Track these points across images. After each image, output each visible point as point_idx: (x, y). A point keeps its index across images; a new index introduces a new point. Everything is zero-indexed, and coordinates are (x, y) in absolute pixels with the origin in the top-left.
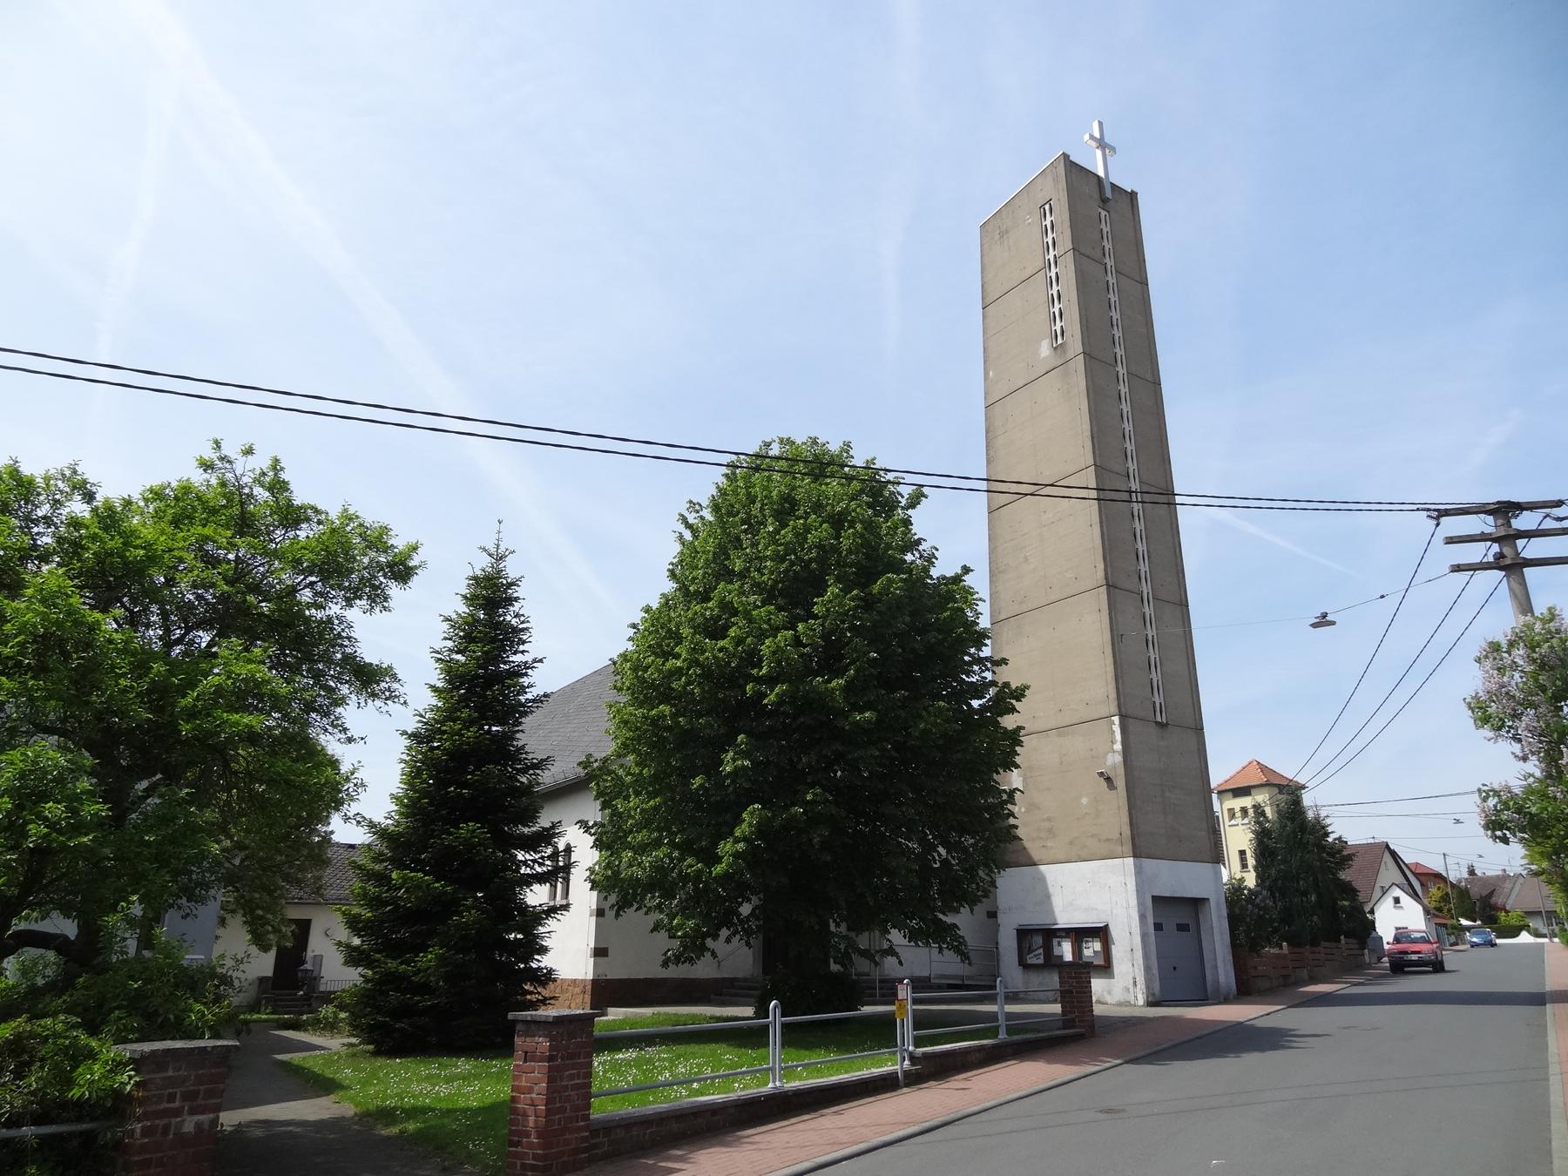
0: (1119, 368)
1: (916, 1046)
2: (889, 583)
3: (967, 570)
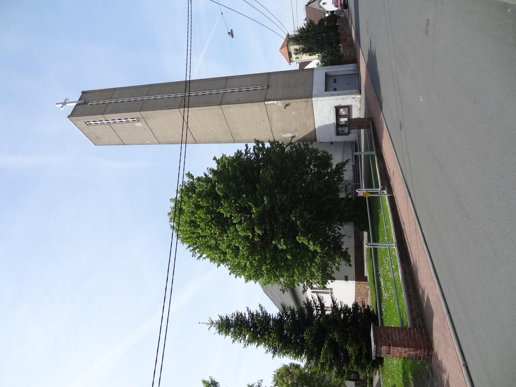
0: (145, 99)
1: (378, 187)
2: (219, 189)
3: (215, 159)
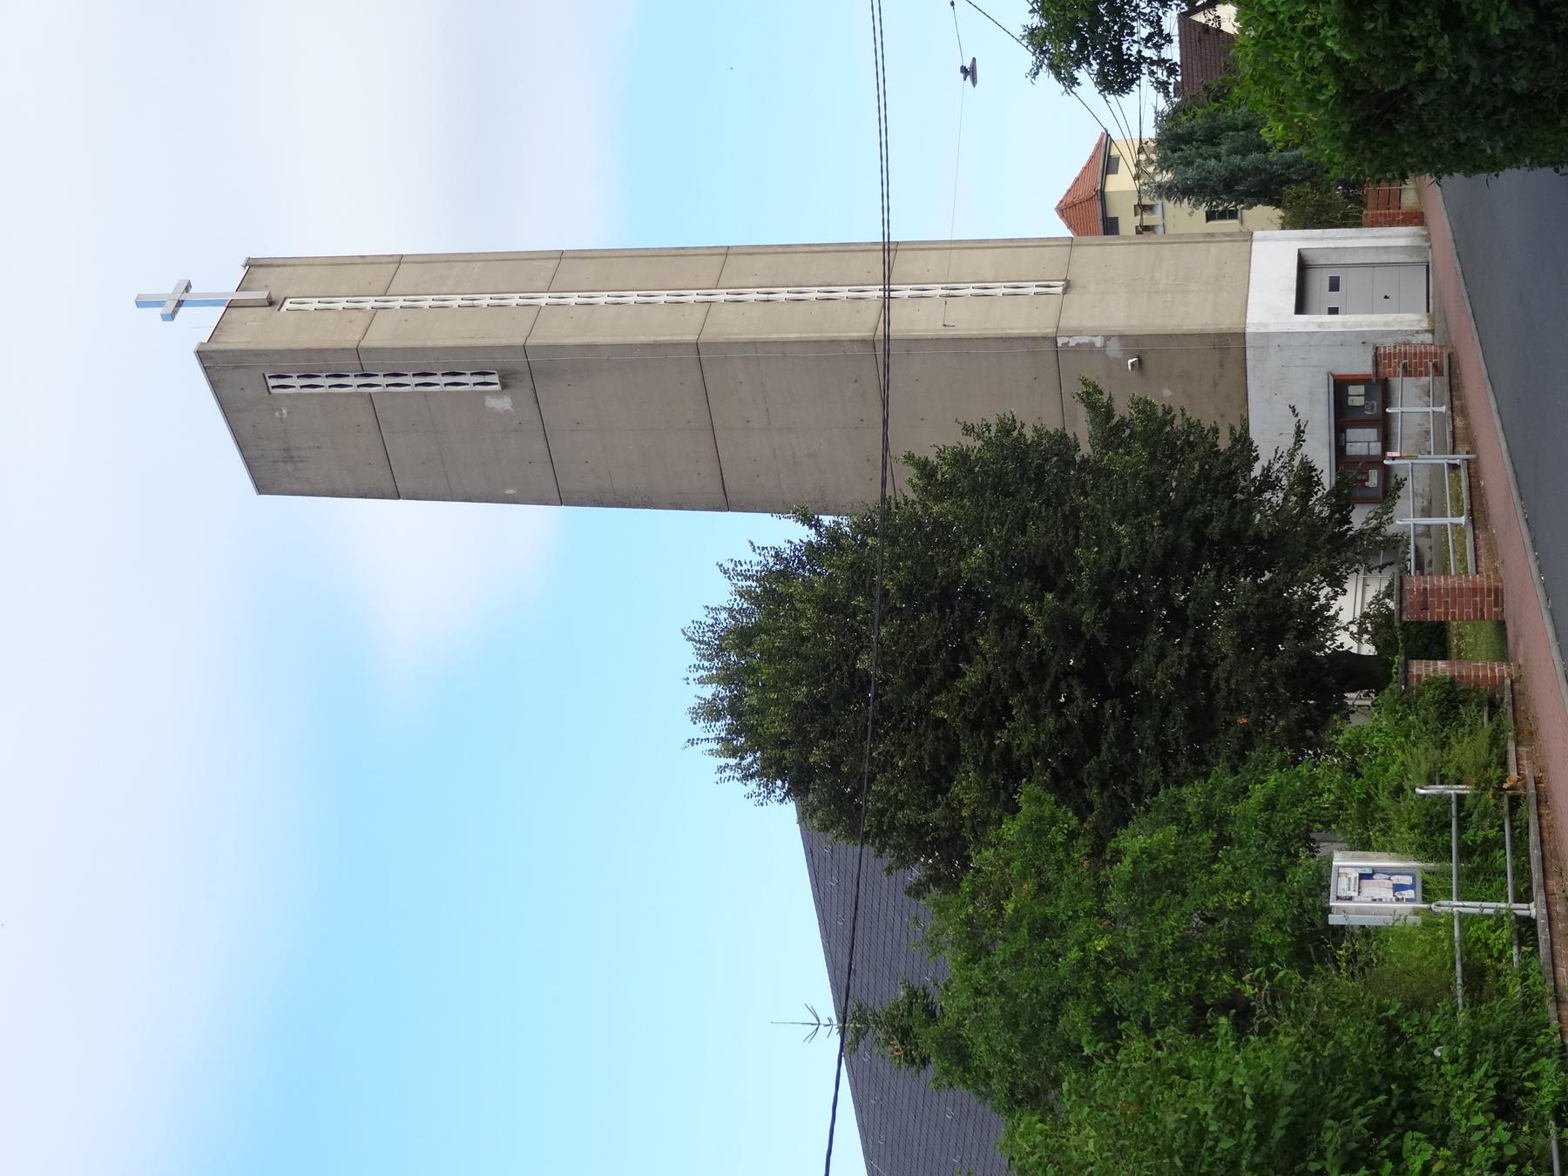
0: (542, 302)
